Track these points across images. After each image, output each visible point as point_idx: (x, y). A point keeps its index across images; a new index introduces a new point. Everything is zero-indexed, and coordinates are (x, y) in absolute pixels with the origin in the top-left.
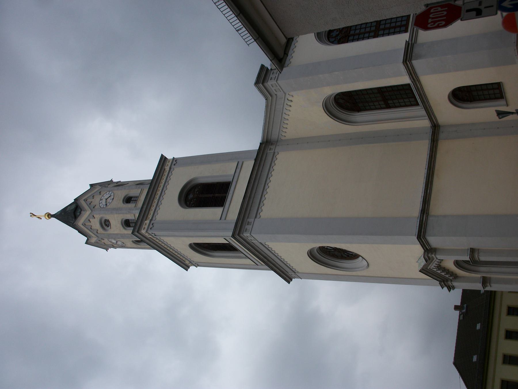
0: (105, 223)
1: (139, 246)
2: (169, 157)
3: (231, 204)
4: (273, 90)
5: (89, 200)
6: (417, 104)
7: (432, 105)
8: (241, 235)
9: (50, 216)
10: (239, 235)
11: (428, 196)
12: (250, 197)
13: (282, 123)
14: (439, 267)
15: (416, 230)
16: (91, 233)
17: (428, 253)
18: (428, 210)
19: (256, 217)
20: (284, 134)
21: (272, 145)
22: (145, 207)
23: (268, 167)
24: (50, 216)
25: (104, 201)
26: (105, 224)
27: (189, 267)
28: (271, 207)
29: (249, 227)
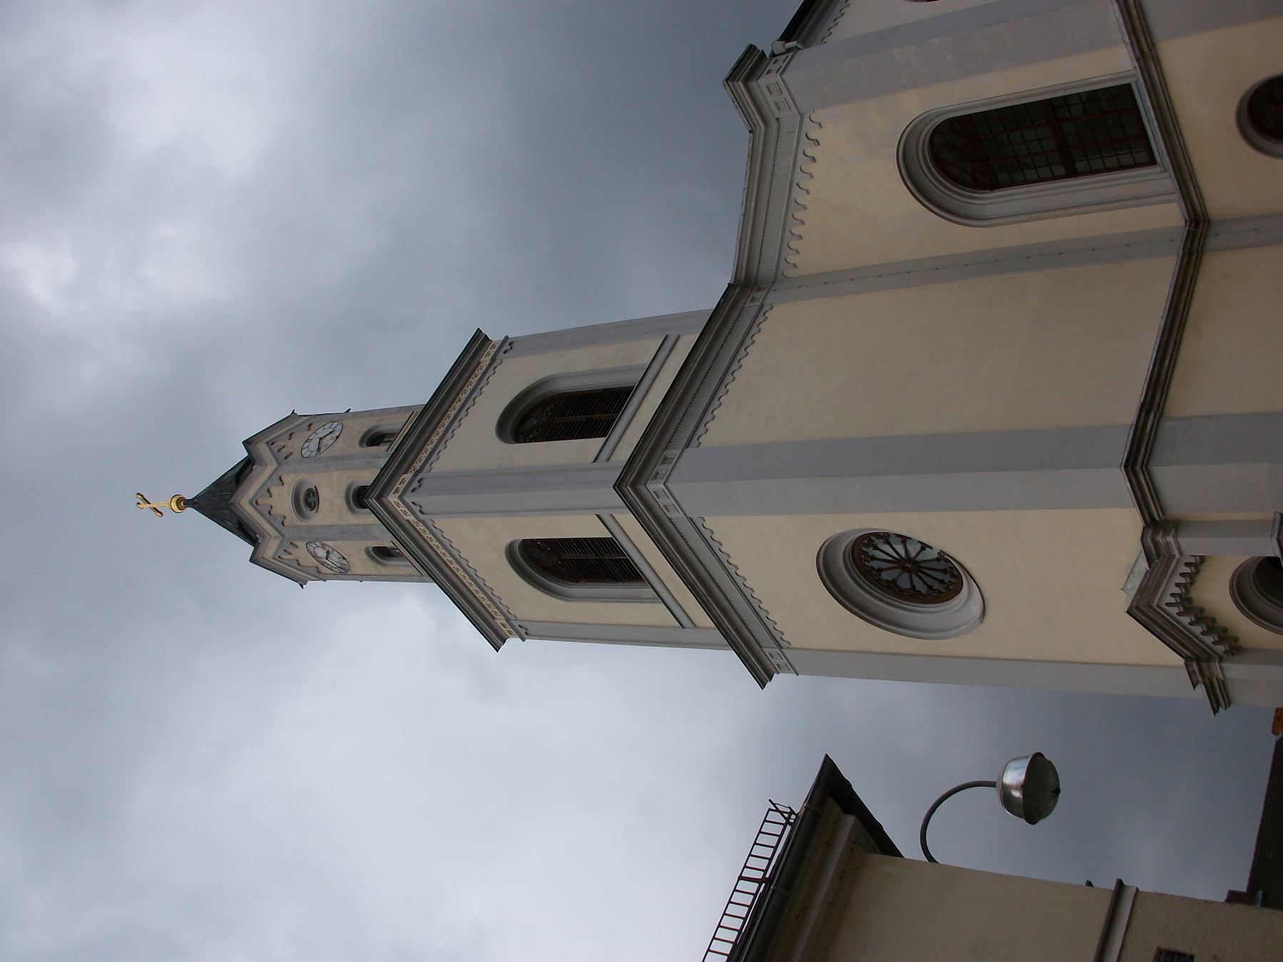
0: (306, 500)
1: (383, 570)
2: (495, 336)
3: (631, 427)
5: (279, 444)
6: (1152, 162)
7: (1191, 147)
8: (642, 488)
9: (183, 503)
10: (634, 485)
11: (1164, 373)
12: (680, 402)
13: (790, 219)
14: (1185, 602)
15: (1121, 453)
16: (267, 526)
17: (1155, 533)
19: (687, 445)
20: (791, 259)
21: (759, 289)
22: (411, 441)
24: (183, 503)
25: (313, 445)
26: (308, 500)
27: (504, 641)
28: (733, 421)
29: (663, 469)
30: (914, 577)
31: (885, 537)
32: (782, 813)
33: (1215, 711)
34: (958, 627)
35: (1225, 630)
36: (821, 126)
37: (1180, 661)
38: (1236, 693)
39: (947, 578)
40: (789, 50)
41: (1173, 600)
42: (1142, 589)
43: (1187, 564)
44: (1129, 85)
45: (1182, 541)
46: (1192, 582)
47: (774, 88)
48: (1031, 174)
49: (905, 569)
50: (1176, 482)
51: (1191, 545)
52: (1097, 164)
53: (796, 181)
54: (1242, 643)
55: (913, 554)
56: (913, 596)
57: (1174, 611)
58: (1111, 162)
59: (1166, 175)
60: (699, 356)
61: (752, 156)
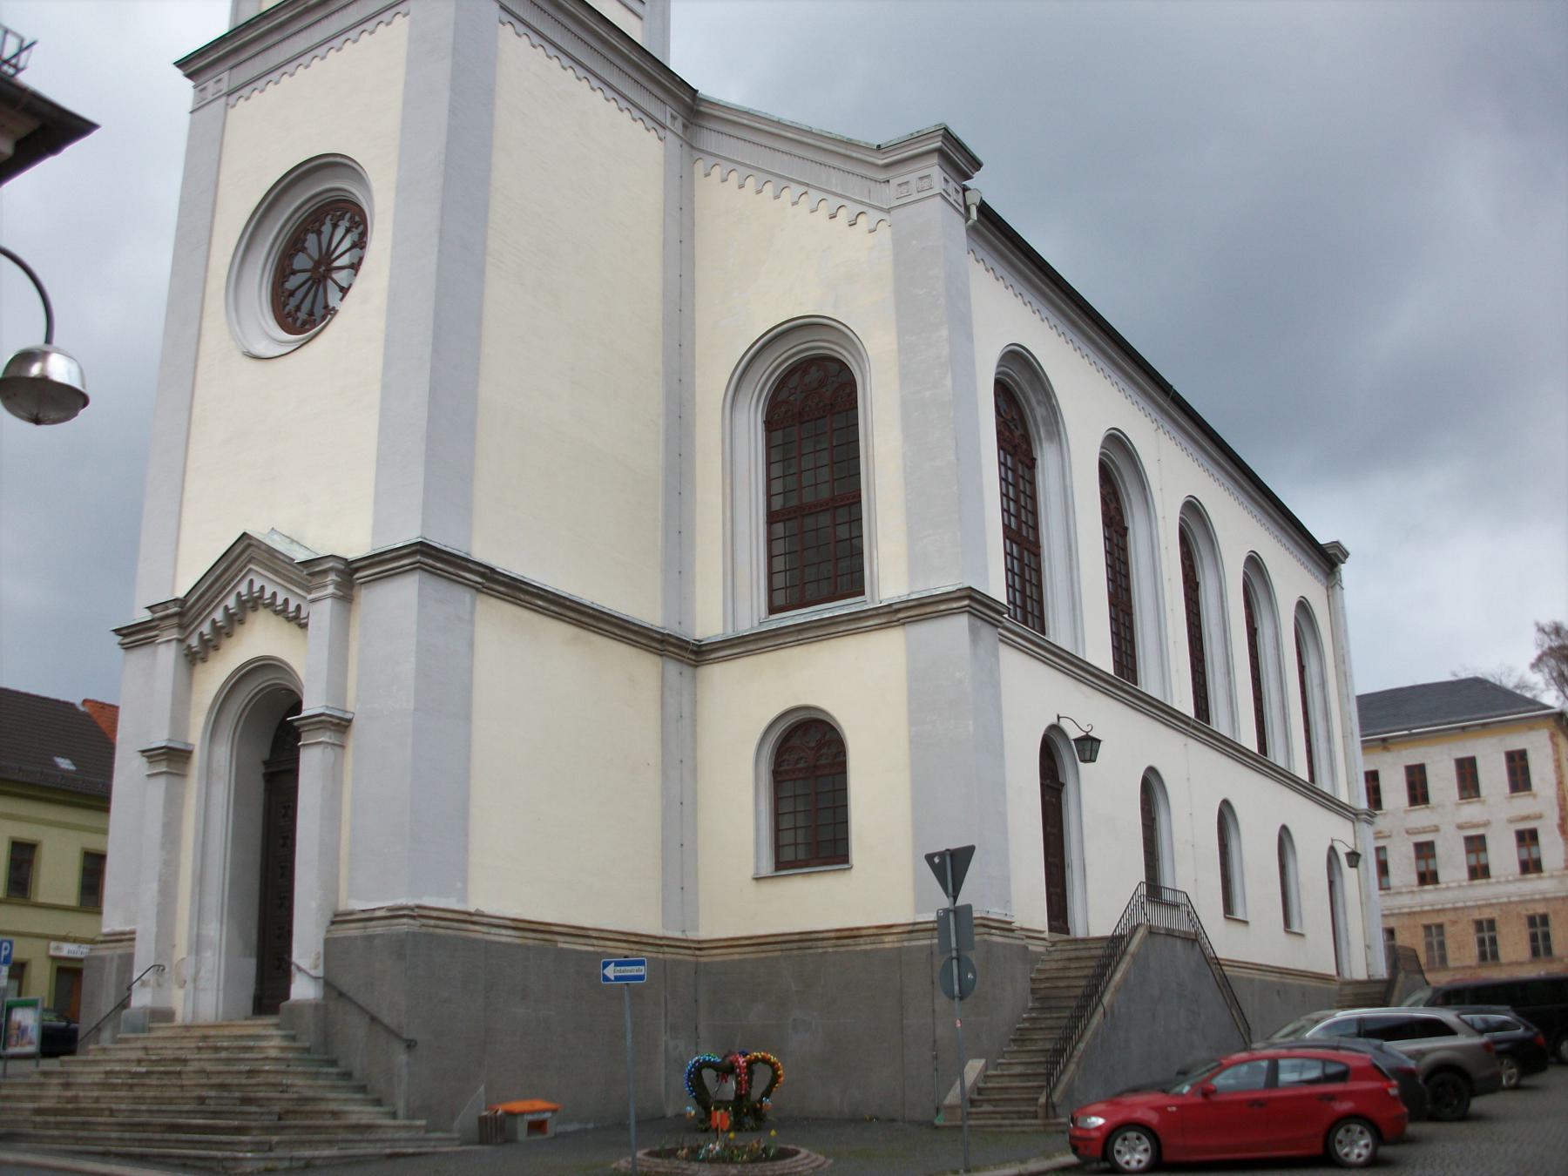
4: (911, 174)
6: (773, 610)
11: (527, 598)
14: (253, 603)
15: (437, 540)
17: (339, 572)
18: (490, 592)
20: (716, 172)
21: (685, 126)
23: (621, 88)
30: (307, 275)
31: (360, 244)
32: (16, 56)
33: (117, 631)
34: (239, 323)
35: (216, 648)
36: (871, 231)
37: (181, 593)
38: (139, 657)
39: (302, 315)
40: (967, 209)
41: (256, 588)
42: (271, 552)
43: (298, 608)
44: (862, 593)
45: (329, 602)
46: (277, 613)
47: (926, 183)
48: (777, 471)
49: (317, 264)
50: (402, 596)
51: (322, 613)
52: (779, 547)
53: (811, 192)
54: (200, 667)
55: (337, 276)
56: (283, 271)
57: (243, 588)
58: (779, 564)
59: (756, 623)
60: (614, 40)
61: (849, 143)
